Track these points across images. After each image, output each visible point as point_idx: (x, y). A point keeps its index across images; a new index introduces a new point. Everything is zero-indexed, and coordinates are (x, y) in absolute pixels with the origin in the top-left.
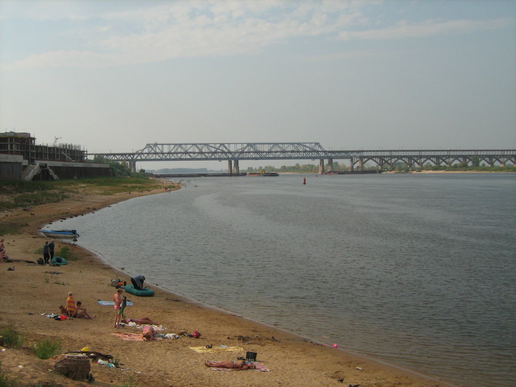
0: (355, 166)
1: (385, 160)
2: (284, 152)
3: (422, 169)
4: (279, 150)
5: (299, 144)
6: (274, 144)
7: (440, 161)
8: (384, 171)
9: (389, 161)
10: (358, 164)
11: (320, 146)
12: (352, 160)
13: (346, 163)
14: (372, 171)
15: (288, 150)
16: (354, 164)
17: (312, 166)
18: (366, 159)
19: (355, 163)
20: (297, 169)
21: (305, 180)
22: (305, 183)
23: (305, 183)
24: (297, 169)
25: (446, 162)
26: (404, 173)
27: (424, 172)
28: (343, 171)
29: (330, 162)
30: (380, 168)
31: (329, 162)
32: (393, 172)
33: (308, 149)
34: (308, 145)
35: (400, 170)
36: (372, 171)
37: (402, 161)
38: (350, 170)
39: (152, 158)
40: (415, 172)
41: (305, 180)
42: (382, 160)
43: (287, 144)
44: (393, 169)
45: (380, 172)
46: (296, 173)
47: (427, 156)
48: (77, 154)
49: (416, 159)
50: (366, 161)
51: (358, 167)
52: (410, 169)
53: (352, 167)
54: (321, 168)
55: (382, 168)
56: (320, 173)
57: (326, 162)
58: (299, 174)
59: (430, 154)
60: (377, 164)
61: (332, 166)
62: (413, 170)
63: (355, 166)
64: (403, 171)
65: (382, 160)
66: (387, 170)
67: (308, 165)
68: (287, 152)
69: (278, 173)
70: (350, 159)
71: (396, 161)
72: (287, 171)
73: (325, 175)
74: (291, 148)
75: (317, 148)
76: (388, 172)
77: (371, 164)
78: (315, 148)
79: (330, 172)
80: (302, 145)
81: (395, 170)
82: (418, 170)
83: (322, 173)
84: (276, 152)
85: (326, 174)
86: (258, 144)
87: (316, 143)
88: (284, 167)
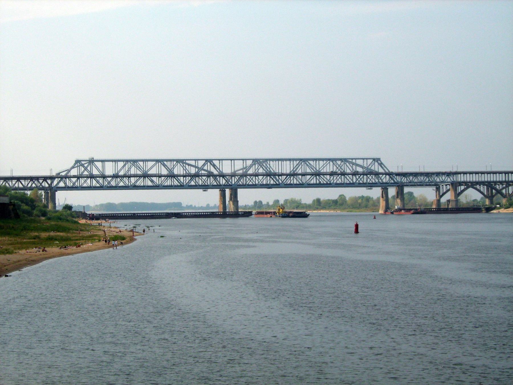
0: (443, 200)
1: (496, 189)
2: (317, 174)
4: (308, 171)
11: (381, 164)
12: (438, 189)
13: (427, 194)
14: (474, 209)
15: (324, 170)
16: (441, 197)
19: (444, 194)
20: (342, 204)
21: (357, 226)
22: (357, 231)
23: (357, 231)
24: (342, 204)
28: (423, 208)
29: (400, 193)
30: (487, 202)
31: (398, 193)
33: (360, 170)
34: (359, 162)
36: (474, 209)
38: (434, 207)
39: (312, 182)
41: (357, 226)
43: (323, 160)
45: (488, 210)
46: (339, 212)
50: (462, 191)
51: (449, 201)
53: (439, 201)
54: (382, 203)
55: (492, 202)
56: (381, 211)
57: (392, 192)
58: (345, 213)
59: (475, 178)
61: (403, 199)
63: (443, 200)
69: (308, 212)
74: (330, 168)
75: (376, 168)
76: (502, 211)
77: (472, 195)
78: (373, 168)
79: (399, 210)
83: (386, 210)
84: (303, 175)
85: (392, 213)
87: (374, 160)
88: (318, 200)
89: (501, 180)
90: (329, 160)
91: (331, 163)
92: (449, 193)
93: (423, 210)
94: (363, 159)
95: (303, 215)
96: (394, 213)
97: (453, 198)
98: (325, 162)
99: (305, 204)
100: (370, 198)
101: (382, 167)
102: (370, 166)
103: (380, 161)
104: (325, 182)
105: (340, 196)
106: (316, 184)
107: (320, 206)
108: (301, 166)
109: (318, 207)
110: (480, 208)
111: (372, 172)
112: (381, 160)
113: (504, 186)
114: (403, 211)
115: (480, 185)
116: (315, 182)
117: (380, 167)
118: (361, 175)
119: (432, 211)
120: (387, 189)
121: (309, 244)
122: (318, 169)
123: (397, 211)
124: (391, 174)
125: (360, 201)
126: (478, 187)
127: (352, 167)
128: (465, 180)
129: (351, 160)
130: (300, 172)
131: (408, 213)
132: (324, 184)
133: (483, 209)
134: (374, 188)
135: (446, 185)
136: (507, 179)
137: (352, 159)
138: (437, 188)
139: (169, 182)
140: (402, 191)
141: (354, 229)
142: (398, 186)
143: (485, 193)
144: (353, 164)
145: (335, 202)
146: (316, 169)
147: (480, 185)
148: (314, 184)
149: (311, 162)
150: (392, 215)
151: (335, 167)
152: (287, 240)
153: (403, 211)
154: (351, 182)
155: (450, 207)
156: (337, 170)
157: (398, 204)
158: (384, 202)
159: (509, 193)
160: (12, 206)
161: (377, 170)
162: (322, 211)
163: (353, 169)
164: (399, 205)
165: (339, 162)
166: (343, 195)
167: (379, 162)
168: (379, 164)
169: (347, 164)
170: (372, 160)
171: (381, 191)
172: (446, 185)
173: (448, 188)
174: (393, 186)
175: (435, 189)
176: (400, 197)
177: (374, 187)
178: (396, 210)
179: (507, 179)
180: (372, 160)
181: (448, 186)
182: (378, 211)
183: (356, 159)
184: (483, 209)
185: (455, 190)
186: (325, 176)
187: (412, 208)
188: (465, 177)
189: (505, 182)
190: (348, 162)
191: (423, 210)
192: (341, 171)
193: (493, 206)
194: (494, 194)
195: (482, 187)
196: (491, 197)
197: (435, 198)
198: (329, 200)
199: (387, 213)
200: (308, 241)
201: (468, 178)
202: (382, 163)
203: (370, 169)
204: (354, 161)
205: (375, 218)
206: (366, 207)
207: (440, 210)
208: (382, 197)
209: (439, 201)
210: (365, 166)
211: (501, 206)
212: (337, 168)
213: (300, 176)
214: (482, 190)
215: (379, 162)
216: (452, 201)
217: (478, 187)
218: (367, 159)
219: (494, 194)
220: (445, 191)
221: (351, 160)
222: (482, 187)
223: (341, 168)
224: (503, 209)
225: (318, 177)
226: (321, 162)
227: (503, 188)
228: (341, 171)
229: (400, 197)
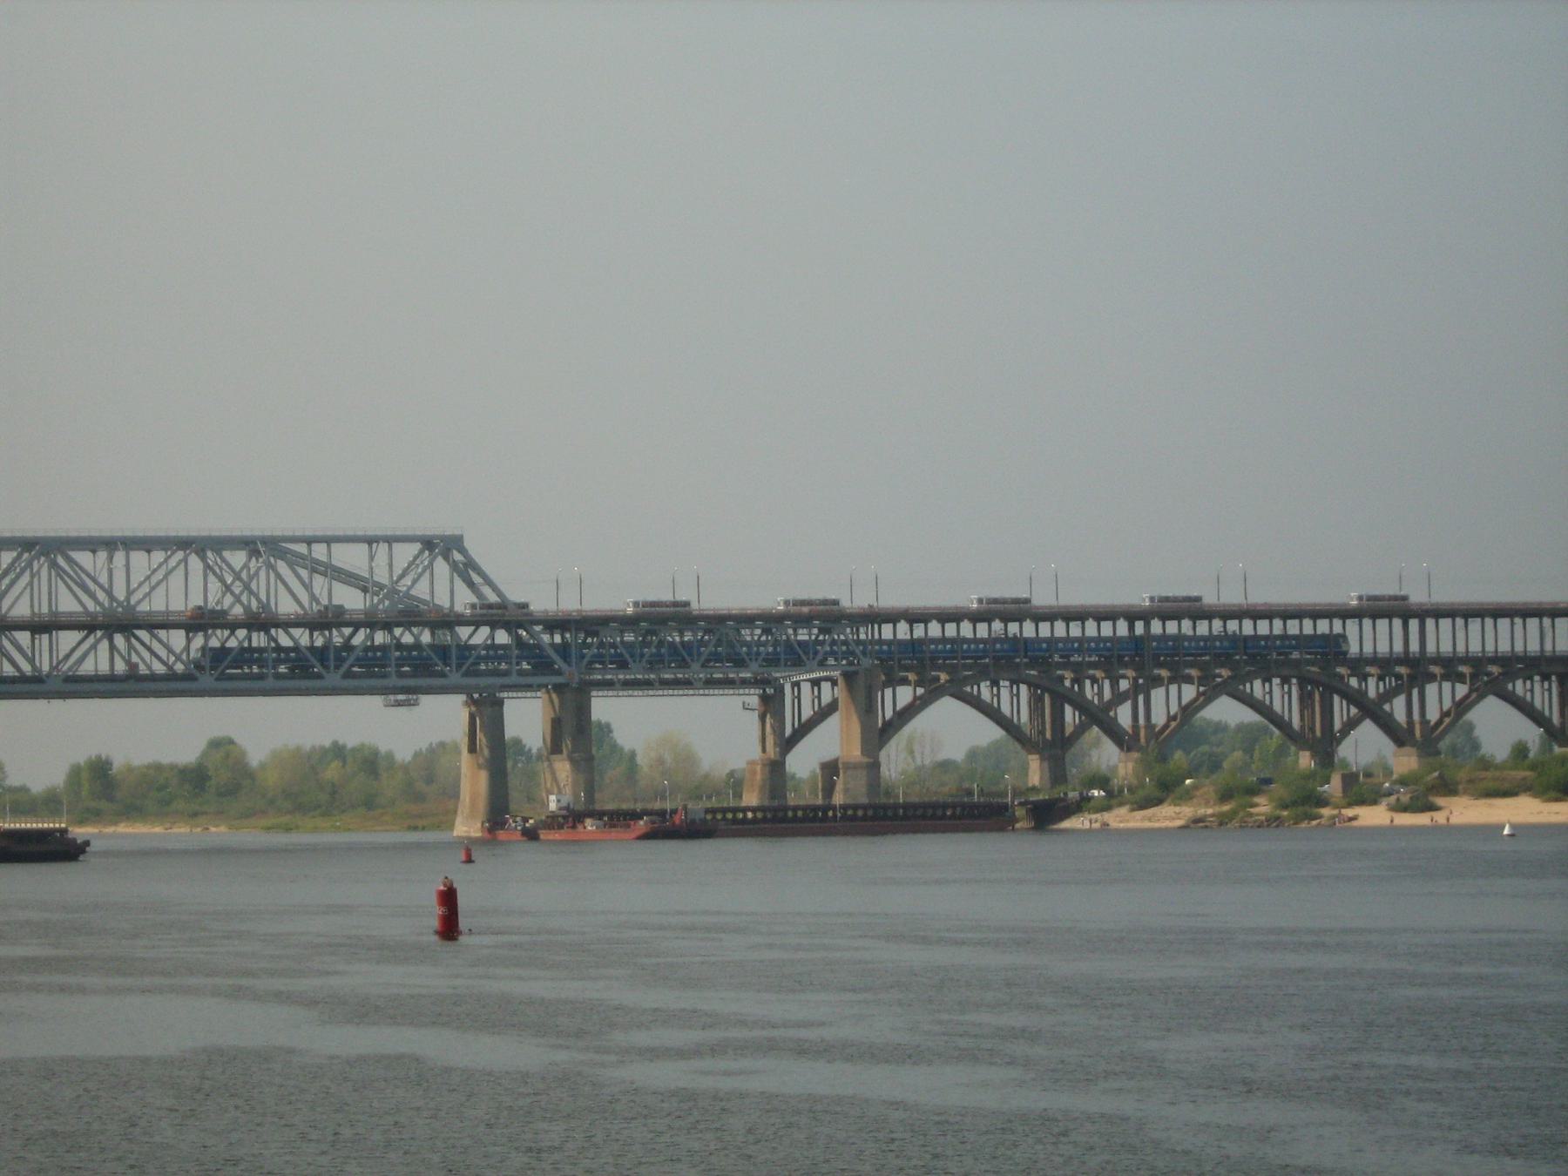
0: (803, 762)
1: (1081, 705)
2: (119, 623)
3: (1448, 788)
4: (68, 604)
5: (262, 547)
6: (27, 545)
7: (1341, 710)
8: (1081, 806)
9: (1124, 715)
10: (833, 740)
11: (467, 570)
12: (771, 705)
13: (703, 732)
14: (966, 810)
15: (156, 604)
16: (788, 744)
17: (371, 762)
18: (905, 695)
19: (803, 729)
20: (231, 791)
21: (448, 897)
22: (449, 928)
23: (449, 928)
24: (231, 791)
25: (1387, 725)
26: (1273, 821)
27: (1464, 811)
28: (697, 807)
29: (574, 731)
30: (1035, 772)
31: (556, 725)
32: (1169, 815)
33: (351, 600)
34: (351, 557)
35: (1238, 792)
36: (966, 810)
37: (1249, 716)
38: (751, 799)
39: (87, 668)
40: (1374, 816)
41: (448, 897)
42: (1060, 699)
43: (147, 544)
44: (1166, 790)
45: (1046, 814)
46: (219, 832)
47: (1478, 663)
48: (680, 615)
49: (1372, 689)
50: (905, 715)
51: (831, 769)
52: (1334, 787)
53: (776, 768)
54: (473, 783)
55: (1058, 775)
56: (467, 826)
57: (527, 718)
58: (250, 836)
59: (1502, 638)
60: (994, 732)
61: (586, 764)
62: (1361, 790)
63: (803, 762)
64: (1263, 806)
65: (1060, 699)
66: (1113, 798)
67: (149, 767)
68: (155, 624)
69: (79, 832)
70: (463, 697)
71: (1188, 710)
72: (132, 811)
73: (527, 854)
74: (189, 586)
75: (443, 590)
76: (1121, 818)
77: (950, 734)
78: (421, 590)
79: (572, 817)
80: (295, 561)
81: (1187, 797)
82: (1405, 796)
83: (497, 817)
84: (39, 627)
85: (531, 835)
86: (92, 544)
87: (428, 544)
88: (100, 770)
89: (1383, 648)
90: (185, 544)
91: (194, 561)
92: (833, 723)
93: (688, 820)
94: (370, 541)
95: (56, 850)
96: (543, 834)
97: (855, 753)
98: (158, 556)
99: (24, 789)
100: (375, 753)
101: (471, 585)
102: (408, 581)
103: (463, 551)
104: (159, 668)
105: (215, 744)
106: (112, 678)
107: (111, 799)
108: (25, 579)
109: (104, 805)
110: (1005, 807)
111: (419, 614)
112: (467, 544)
113: (1124, 685)
114: (590, 825)
115: (995, 683)
116: (104, 668)
117: (460, 585)
118: (357, 626)
119: (745, 821)
120: (500, 703)
121: (280, 997)
122: (120, 594)
123: (553, 822)
124: (520, 625)
125: (332, 772)
126: (1519, 687)
127: (308, 587)
128: (1519, 648)
129: (302, 548)
130: (22, 610)
131: (614, 833)
132: (153, 677)
133: (1020, 812)
134: (425, 700)
135: (816, 683)
136: (1414, 647)
137: (309, 541)
138: (765, 699)
139: (100, 660)
140: (583, 710)
141: (432, 916)
142: (558, 688)
143: (1296, 723)
144: (316, 567)
145: (195, 779)
146: (112, 598)
147: (995, 683)
148: (96, 679)
149: (83, 558)
150: (534, 845)
151: (214, 586)
152: (118, 981)
153: (590, 825)
154: (26, 668)
155: (838, 799)
156: (228, 600)
157: (558, 788)
158: (483, 777)
159: (1424, 721)
160: (335, 764)
161: (442, 600)
162: (122, 828)
163: (313, 598)
164: (568, 790)
165: (237, 558)
166: (231, 742)
167: (457, 556)
168: (454, 566)
169: (282, 567)
170: (418, 546)
171: (464, 715)
172: (816, 683)
173: (826, 698)
174: (529, 687)
175: (754, 701)
176: (567, 744)
177: (429, 691)
178: (553, 817)
179: (1414, 647)
180: (416, 548)
181: (826, 686)
182: (451, 827)
183: (329, 541)
184: (1020, 812)
185: (868, 709)
186: (162, 633)
187: (639, 807)
188: (1460, 635)
189: (1406, 660)
190: (283, 554)
191: (688, 820)
192: (247, 609)
193: (1073, 795)
194: (1069, 730)
195: (1005, 693)
196: (1057, 748)
197: (755, 752)
198: (158, 767)
199: (501, 835)
200: (279, 984)
201: (1476, 639)
202: (471, 564)
203: (407, 595)
204: (319, 551)
205: (469, 860)
206: (370, 803)
207: (782, 818)
208: (472, 749)
209: (776, 768)
210: (382, 576)
211: (1110, 794)
212: (228, 588)
213: (23, 637)
214: (1006, 709)
215: (457, 556)
216: (849, 766)
217: (1519, 687)
218: (390, 540)
219: (1069, 730)
220: (807, 713)
221: (302, 548)
222: (1005, 693)
223: (247, 587)
224: (1123, 811)
225: (119, 640)
226: (138, 557)
227: (1119, 698)
228: (247, 609)
229: (567, 744)
